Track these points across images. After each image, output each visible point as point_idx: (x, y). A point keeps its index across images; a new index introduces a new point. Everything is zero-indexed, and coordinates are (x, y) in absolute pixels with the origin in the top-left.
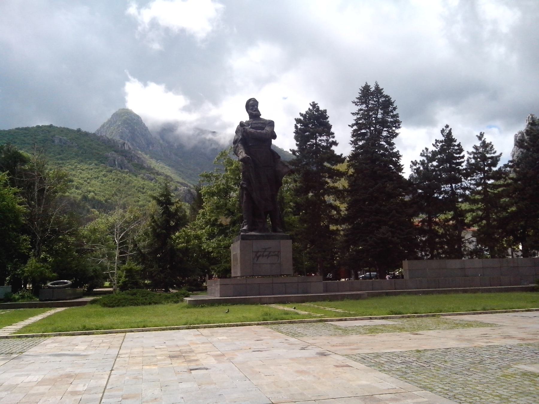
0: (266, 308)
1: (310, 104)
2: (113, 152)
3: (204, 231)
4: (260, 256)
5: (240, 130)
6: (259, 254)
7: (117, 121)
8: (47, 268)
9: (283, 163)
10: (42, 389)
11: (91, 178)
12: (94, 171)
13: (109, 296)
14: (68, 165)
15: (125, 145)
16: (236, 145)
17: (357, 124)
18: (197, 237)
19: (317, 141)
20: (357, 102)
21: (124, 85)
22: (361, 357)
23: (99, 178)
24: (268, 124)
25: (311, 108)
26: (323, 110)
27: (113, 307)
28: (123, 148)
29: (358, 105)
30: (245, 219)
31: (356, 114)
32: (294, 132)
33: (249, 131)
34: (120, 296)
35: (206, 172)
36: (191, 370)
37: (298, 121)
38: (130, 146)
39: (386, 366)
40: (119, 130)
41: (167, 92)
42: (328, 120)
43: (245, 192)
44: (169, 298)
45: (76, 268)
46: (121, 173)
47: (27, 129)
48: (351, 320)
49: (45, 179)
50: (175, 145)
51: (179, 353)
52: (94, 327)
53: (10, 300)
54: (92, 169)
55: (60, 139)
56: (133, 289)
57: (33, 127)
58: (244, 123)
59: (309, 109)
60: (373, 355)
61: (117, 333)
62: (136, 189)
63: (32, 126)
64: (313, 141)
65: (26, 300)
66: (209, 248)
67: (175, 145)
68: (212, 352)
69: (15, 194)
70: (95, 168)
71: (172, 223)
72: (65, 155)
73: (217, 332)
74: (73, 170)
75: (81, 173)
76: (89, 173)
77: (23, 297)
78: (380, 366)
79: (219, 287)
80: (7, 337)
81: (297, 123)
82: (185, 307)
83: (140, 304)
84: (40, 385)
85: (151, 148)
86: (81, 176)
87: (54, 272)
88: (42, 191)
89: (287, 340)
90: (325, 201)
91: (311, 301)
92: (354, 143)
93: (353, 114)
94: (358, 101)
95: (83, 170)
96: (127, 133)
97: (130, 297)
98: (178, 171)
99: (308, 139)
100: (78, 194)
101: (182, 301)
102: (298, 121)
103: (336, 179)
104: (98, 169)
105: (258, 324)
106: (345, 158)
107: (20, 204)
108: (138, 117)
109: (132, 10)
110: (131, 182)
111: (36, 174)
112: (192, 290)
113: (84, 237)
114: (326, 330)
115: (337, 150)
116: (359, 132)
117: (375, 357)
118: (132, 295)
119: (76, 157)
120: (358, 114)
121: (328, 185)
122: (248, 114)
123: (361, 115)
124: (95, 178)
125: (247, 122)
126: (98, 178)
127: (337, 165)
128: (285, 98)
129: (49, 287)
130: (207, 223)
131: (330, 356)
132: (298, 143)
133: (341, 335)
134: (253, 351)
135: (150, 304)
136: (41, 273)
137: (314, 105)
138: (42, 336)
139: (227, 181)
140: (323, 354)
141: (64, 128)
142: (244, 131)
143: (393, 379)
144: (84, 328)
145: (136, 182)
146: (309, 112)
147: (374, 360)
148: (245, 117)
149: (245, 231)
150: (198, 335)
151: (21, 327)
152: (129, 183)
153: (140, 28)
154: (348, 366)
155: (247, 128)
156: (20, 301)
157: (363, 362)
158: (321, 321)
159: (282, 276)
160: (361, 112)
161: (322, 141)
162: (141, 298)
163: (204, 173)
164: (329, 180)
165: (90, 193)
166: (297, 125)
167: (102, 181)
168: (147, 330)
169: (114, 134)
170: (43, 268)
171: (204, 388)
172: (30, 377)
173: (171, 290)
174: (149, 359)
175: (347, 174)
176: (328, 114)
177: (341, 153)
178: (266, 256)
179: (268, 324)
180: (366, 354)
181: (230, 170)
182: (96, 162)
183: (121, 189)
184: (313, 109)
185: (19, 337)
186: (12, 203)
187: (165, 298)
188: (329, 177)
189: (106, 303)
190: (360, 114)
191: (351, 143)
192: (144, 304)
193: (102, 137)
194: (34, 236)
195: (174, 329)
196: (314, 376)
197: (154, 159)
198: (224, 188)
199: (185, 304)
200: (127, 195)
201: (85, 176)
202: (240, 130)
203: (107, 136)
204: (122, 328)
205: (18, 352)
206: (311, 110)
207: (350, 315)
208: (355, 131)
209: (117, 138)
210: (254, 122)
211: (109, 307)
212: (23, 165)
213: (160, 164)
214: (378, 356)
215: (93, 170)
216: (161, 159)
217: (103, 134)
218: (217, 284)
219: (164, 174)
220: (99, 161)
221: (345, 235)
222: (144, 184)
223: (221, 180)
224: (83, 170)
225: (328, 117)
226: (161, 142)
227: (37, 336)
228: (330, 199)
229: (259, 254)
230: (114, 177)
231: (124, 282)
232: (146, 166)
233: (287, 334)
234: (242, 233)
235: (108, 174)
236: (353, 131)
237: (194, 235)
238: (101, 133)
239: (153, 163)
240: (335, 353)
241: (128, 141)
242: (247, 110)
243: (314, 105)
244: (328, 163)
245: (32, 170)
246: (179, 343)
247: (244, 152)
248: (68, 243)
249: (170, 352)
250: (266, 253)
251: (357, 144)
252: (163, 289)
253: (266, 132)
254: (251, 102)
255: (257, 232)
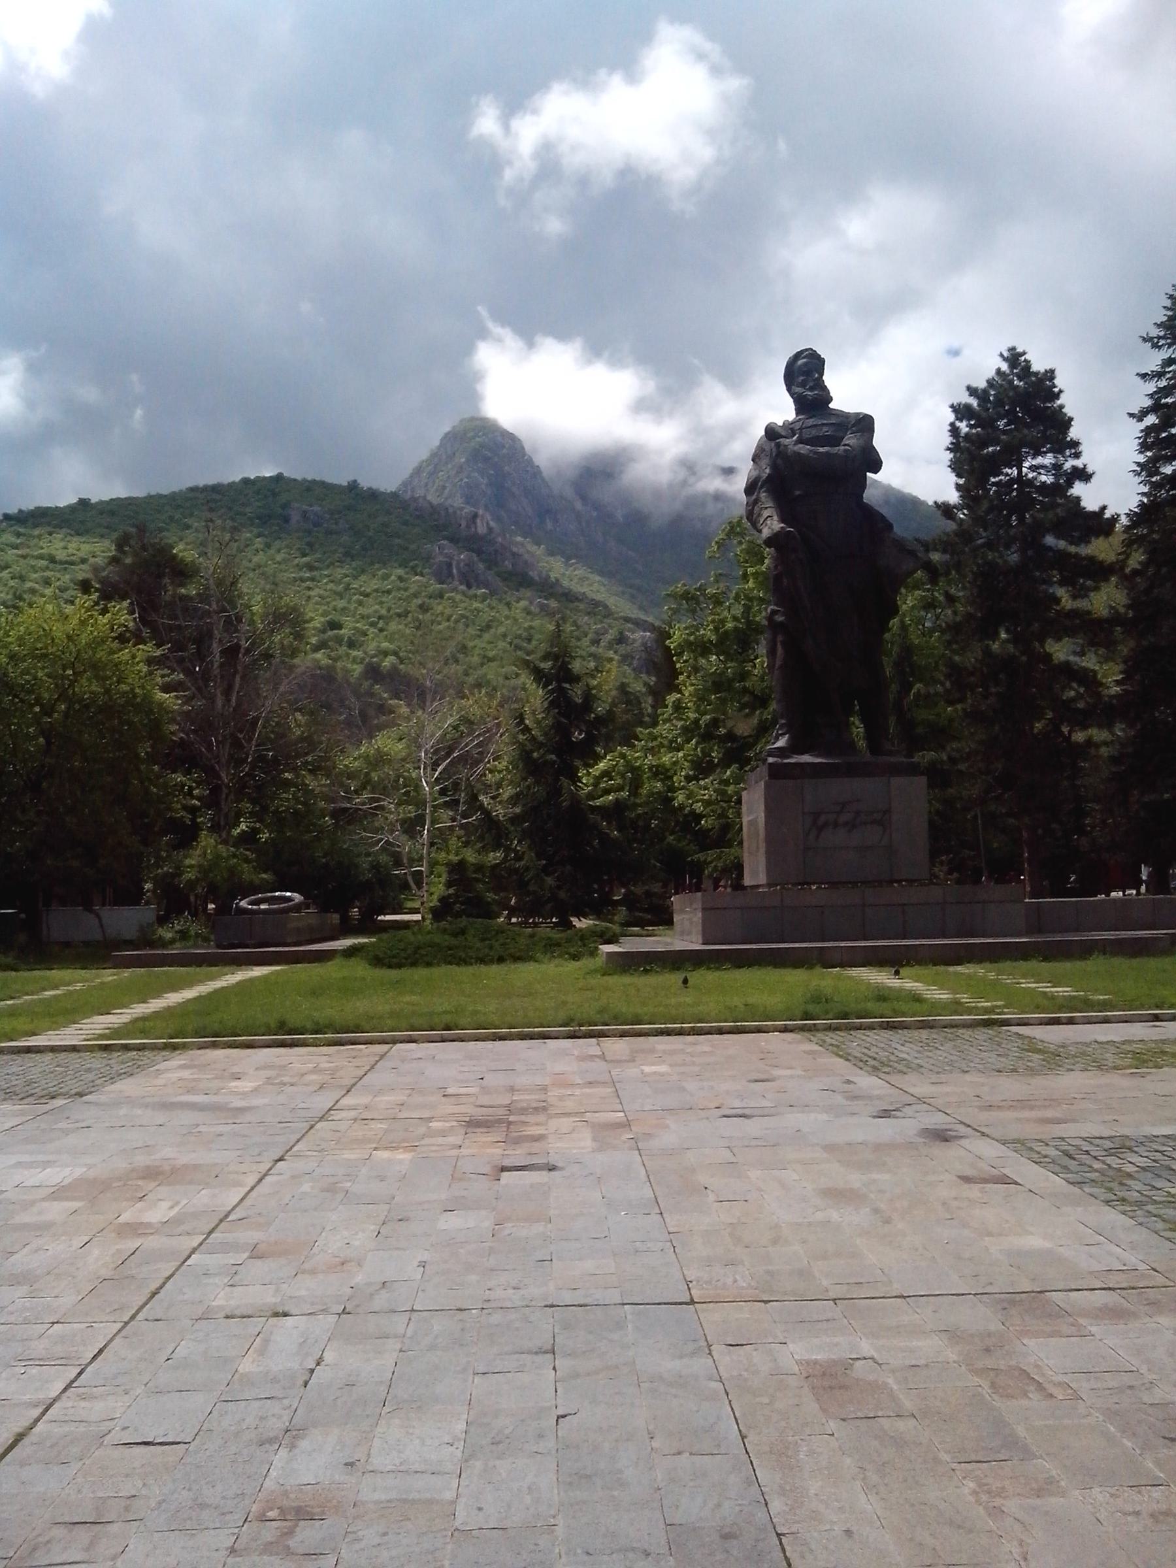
0: (826, 980)
1: (1001, 355)
2: (445, 542)
3: (681, 754)
4: (826, 824)
5: (767, 448)
6: (823, 818)
7: (457, 454)
8: (247, 860)
9: (900, 545)
10: (56, 1211)
11: (389, 615)
12: (394, 598)
13: (395, 936)
14: (326, 584)
15: (478, 521)
16: (754, 497)
17: (1155, 408)
18: (660, 772)
19: (1024, 470)
20: (1159, 338)
21: (468, 350)
22: (1063, 1151)
23: (410, 615)
24: (853, 426)
25: (1005, 367)
26: (1042, 371)
27: (399, 966)
28: (473, 529)
29: (1160, 347)
30: (782, 718)
31: (1154, 376)
32: (948, 449)
33: (795, 452)
34: (420, 937)
35: (684, 585)
36: (504, 1169)
37: (961, 411)
38: (492, 524)
39: (1138, 1186)
40: (462, 480)
41: (589, 362)
42: (1059, 402)
43: (780, 638)
44: (558, 945)
45: (324, 860)
46: (467, 600)
47: (216, 489)
48: (1089, 1021)
49: (239, 619)
50: (619, 515)
51: (501, 1111)
52: (309, 1025)
53: (151, 944)
54: (389, 592)
55: (305, 512)
56: (459, 919)
57: (233, 483)
58: (778, 429)
59: (999, 371)
60: (1108, 1144)
61: (371, 1043)
62: (511, 644)
63: (230, 480)
64: (1009, 471)
65: (191, 943)
66: (693, 803)
67: (619, 515)
68: (597, 1115)
69: (150, 661)
70: (399, 589)
71: (578, 736)
72: (318, 555)
73: (652, 1051)
74: (341, 595)
75: (360, 603)
76: (381, 603)
77: (183, 935)
78: (1115, 1185)
79: (700, 915)
80: (74, 1049)
81: (957, 419)
82: (596, 971)
83: (473, 961)
84: (55, 1199)
85: (549, 525)
86: (361, 610)
87: (265, 872)
88: (232, 652)
89: (849, 1082)
90: (1048, 657)
91: (980, 960)
92: (1148, 469)
93: (1144, 376)
94: (1162, 334)
95: (367, 595)
96: (483, 487)
97: (448, 940)
98: (631, 587)
99: (994, 465)
100: (354, 661)
101: (593, 953)
102: (961, 411)
103: (1083, 587)
104: (406, 590)
105: (785, 1030)
106: (1115, 519)
107: (166, 689)
108: (511, 437)
109: (487, 123)
110: (495, 624)
111: (214, 606)
112: (642, 924)
113: (351, 776)
114: (993, 1055)
115: (1089, 496)
116: (1164, 435)
117: (1110, 1152)
118: (455, 935)
119: (349, 559)
120: (1159, 375)
121: (1058, 608)
122: (792, 400)
123: (1170, 379)
124: (399, 615)
125: (789, 428)
126: (406, 616)
127: (1089, 542)
128: (955, 353)
129: (245, 911)
130: (688, 732)
131: (963, 1142)
132: (961, 481)
133: (1032, 1071)
134: (725, 1116)
135: (501, 960)
136: (232, 871)
137: (1014, 358)
138: (165, 1047)
139: (747, 609)
140: (942, 1136)
141: (314, 482)
142: (779, 454)
143: (1141, 1235)
144: (283, 1027)
145: (508, 622)
146: (1000, 382)
147: (1104, 1162)
148: (783, 410)
149: (781, 752)
150: (592, 1057)
151: (125, 1019)
152: (489, 626)
153: (509, 174)
154: (1005, 1180)
155: (786, 441)
156: (178, 945)
157: (1065, 1167)
158: (988, 1024)
159: (895, 885)
160: (1171, 369)
161: (1042, 471)
162: (479, 945)
163: (679, 588)
164: (1061, 592)
165: (386, 656)
166: (958, 424)
167: (417, 624)
168: (455, 1037)
169: (447, 491)
170: (235, 860)
171: (507, 1232)
172: (48, 1170)
173: (575, 921)
174: (406, 1130)
175: (1122, 569)
176: (1059, 382)
177: (1101, 504)
178: (846, 824)
179: (818, 1030)
180: (1084, 1139)
181: (756, 575)
182: (400, 572)
183: (471, 644)
184: (1012, 371)
185: (106, 1048)
186: (143, 687)
187: (545, 946)
188: (1062, 583)
189: (381, 955)
190: (1168, 376)
191: (1139, 469)
192: (482, 961)
193: (414, 499)
194: (211, 772)
195: (531, 1037)
196: (876, 1211)
197: (559, 557)
198: (736, 629)
199: (600, 961)
200: (486, 661)
201: (370, 611)
202: (767, 448)
203: (429, 498)
204: (385, 1029)
205: (73, 1092)
206: (1004, 373)
207: (1088, 1005)
208: (1148, 431)
209: (458, 502)
210: (811, 422)
211: (390, 967)
212: (182, 585)
213: (575, 570)
214: (1123, 1146)
215: (393, 594)
216: (576, 557)
217: (419, 493)
218: (695, 906)
219: (587, 597)
220: (407, 570)
221: (1114, 760)
222: (531, 627)
223: (729, 608)
224: (367, 595)
225: (1061, 391)
226: (579, 505)
227: (153, 1048)
228: (1061, 651)
229: (823, 818)
230: (448, 611)
231: (442, 900)
232: (537, 578)
233: (860, 1063)
234: (771, 760)
235: (433, 603)
236: (1142, 431)
237: (651, 767)
238: (413, 490)
239: (556, 569)
240: (983, 1134)
241: (486, 508)
242: (789, 390)
243: (1014, 358)
244: (1059, 536)
245: (204, 597)
246: (522, 1081)
247: (775, 518)
248: (308, 792)
249: (479, 1109)
250: (845, 817)
251: (1157, 473)
252: (554, 920)
253: (845, 451)
254: (800, 362)
255: (817, 756)
